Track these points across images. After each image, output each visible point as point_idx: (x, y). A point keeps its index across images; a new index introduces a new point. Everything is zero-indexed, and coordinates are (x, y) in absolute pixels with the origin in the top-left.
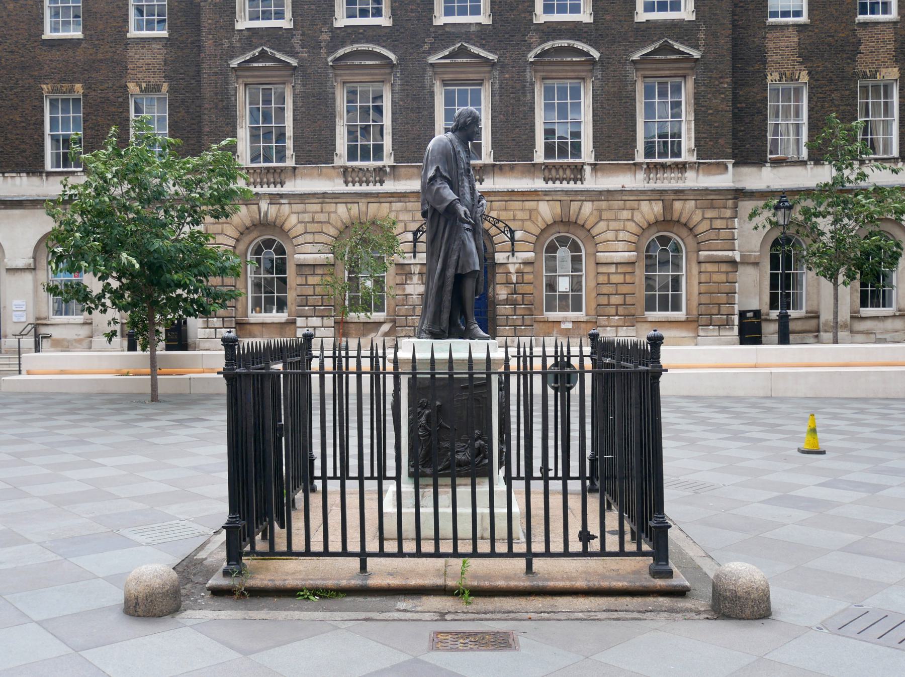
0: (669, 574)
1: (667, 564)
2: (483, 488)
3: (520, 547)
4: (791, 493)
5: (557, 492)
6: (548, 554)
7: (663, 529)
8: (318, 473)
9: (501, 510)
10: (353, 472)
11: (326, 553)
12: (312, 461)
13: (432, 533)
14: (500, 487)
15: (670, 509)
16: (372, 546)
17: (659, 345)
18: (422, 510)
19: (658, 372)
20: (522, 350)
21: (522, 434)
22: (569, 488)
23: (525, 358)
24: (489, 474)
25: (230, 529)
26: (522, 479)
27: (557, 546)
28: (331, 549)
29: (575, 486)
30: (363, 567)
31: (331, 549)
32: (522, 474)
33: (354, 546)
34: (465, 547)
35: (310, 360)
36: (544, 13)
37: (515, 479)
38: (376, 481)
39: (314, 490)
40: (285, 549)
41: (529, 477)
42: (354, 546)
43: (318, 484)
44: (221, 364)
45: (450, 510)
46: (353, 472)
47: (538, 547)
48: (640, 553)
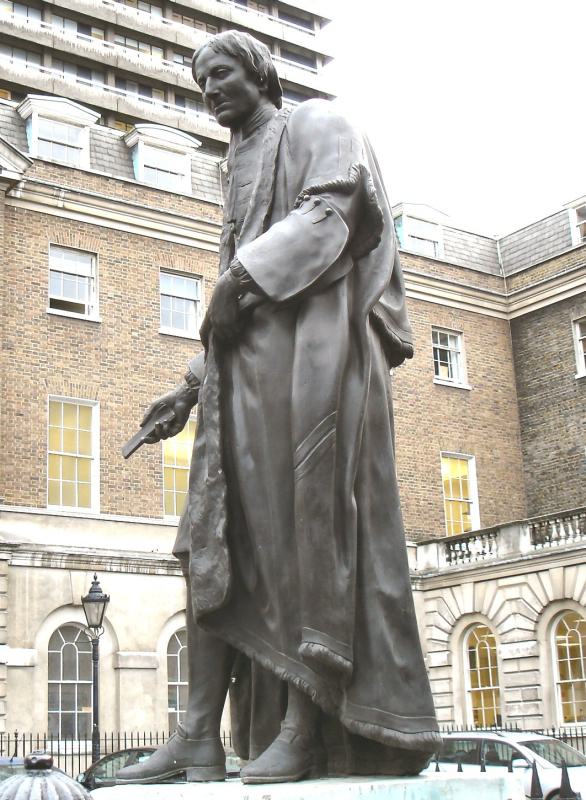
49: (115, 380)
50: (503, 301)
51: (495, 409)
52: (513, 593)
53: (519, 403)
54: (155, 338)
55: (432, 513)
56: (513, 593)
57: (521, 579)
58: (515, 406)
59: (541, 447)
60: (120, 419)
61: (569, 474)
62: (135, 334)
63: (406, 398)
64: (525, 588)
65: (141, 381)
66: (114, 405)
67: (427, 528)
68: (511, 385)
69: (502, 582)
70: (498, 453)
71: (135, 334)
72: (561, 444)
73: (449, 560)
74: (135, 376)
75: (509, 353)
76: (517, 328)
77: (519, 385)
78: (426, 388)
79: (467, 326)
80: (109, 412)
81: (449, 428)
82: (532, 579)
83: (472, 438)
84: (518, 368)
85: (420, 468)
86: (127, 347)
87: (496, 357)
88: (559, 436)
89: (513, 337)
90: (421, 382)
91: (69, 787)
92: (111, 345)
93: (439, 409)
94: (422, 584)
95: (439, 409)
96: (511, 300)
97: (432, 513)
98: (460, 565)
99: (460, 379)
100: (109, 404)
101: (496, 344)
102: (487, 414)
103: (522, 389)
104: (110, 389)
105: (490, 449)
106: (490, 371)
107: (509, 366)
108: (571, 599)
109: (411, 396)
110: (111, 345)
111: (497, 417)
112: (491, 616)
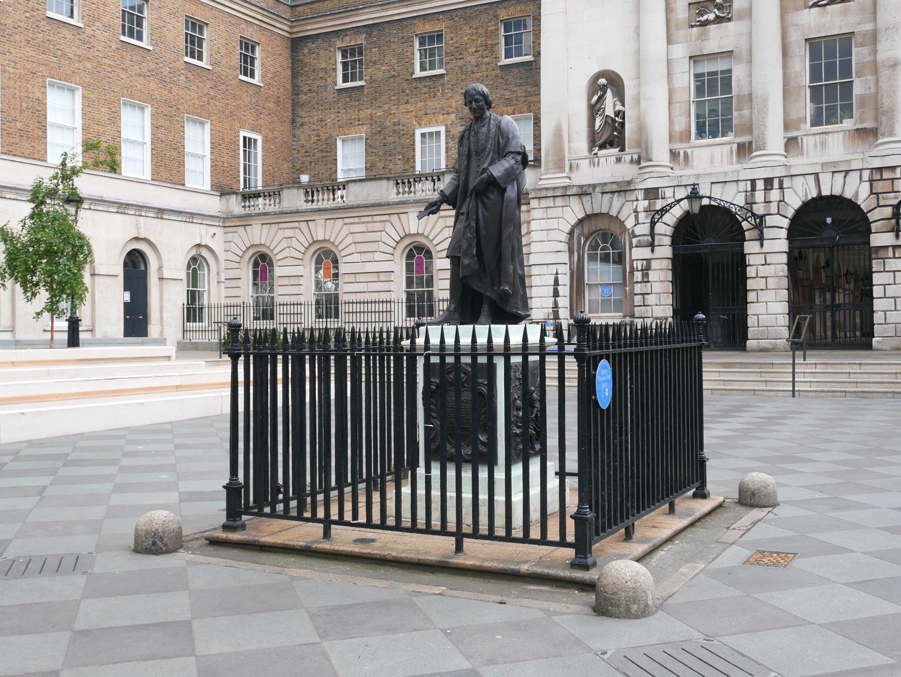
3: (321, 514)
16: (467, 528)
33: (452, 526)
42: (452, 526)
47: (467, 528)
49: (12, 50)
50: (289, 23)
51: (277, 102)
52: (288, 233)
53: (293, 100)
54: (43, 19)
55: (231, 172)
56: (288, 233)
57: (386, 218)
58: (290, 102)
59: (303, 134)
60: (15, 81)
61: (324, 154)
62: (28, 15)
63: (219, 88)
64: (388, 224)
65: (32, 53)
66: (12, 70)
67: (228, 183)
68: (289, 87)
69: (281, 226)
70: (277, 134)
71: (28, 15)
72: (321, 133)
73: (244, 207)
74: (27, 49)
75: (288, 63)
76: (296, 44)
77: (295, 86)
78: (233, 82)
79: (263, 39)
80: (7, 75)
81: (247, 113)
82: (394, 218)
83: (261, 122)
84: (295, 75)
85: (226, 140)
86: (22, 24)
87: (283, 60)
88: (320, 127)
89: (292, 51)
90: (231, 77)
91: (810, 487)
92: (9, 21)
93: (241, 98)
94: (224, 222)
95: (241, 98)
96: (294, 24)
97: (231, 172)
98: (252, 211)
99: (256, 81)
100: (7, 68)
101: (281, 54)
102: (272, 105)
103: (296, 90)
104: (8, 56)
105: (272, 130)
106: (276, 74)
107: (289, 72)
108: (333, 243)
109: (223, 87)
110: (9, 21)
111: (278, 108)
112: (336, 243)
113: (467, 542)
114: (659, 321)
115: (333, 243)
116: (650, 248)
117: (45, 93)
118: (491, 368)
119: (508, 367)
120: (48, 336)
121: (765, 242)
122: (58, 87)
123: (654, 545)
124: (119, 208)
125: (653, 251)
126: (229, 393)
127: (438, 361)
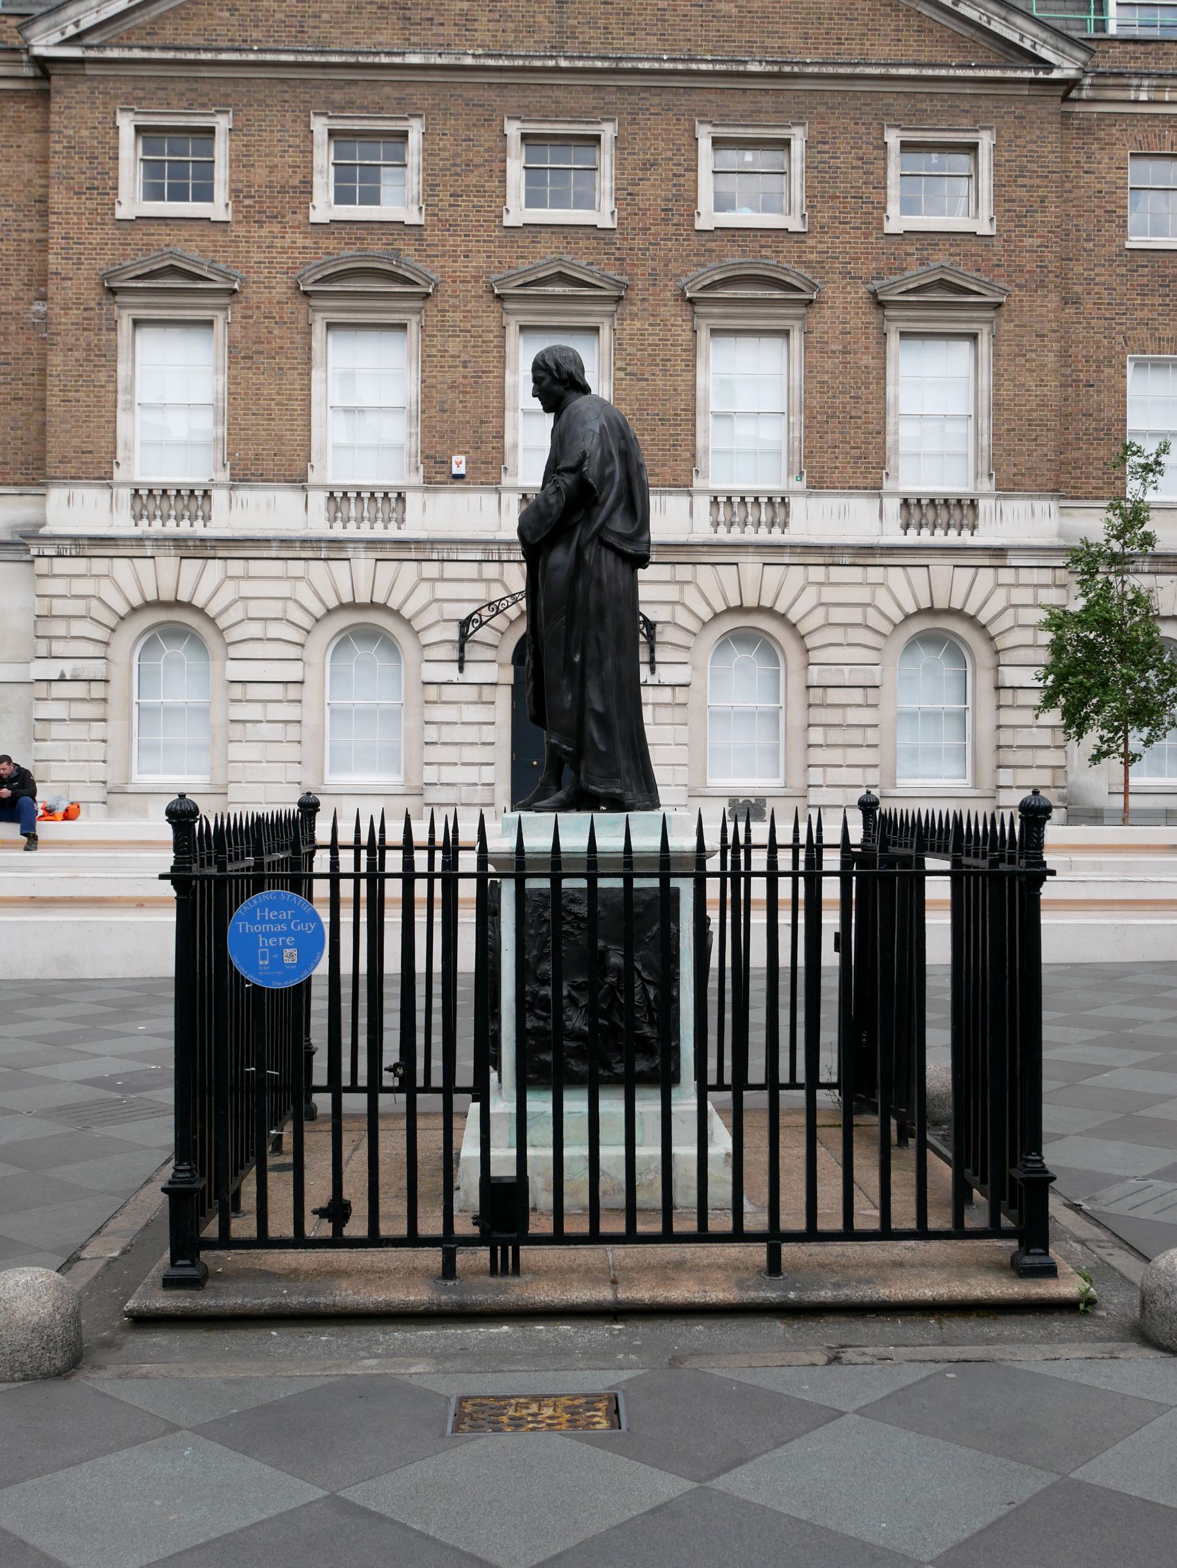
0: (1050, 1271)
1: (1047, 1253)
2: (648, 1106)
3: (430, 1224)
4: (1142, 1113)
5: (395, 1116)
6: (812, 1234)
7: (1041, 1183)
8: (320, 1077)
9: (685, 1150)
10: (756, 1071)
11: (849, 1234)
12: (310, 1053)
13: (621, 1199)
14: (685, 1102)
15: (1052, 1155)
16: (793, 1219)
17: (1041, 824)
18: (530, 1152)
19: (1041, 874)
20: (803, 827)
21: (728, 998)
22: (783, 1105)
23: (202, 866)
24: (667, 1080)
25: (176, 1194)
26: (436, 1090)
27: (830, 1218)
28: (859, 1224)
29: (827, 1099)
30: (774, 1266)
31: (859, 1224)
32: (801, 1078)
33: (756, 1219)
34: (577, 1224)
35: (312, 854)
36: (336, 203)
37: (348, 1090)
38: (365, 1096)
39: (312, 1115)
40: (289, 1232)
41: (740, 1084)
42: (756, 1219)
43: (322, 1102)
44: (166, 859)
45: (567, 1152)
46: (756, 1071)
47: (793, 1219)
48: (994, 1231)
108: (221, 632)
113: (788, 1251)
114: (450, 812)
115: (221, 632)
116: (456, 665)
117: (882, 356)
118: (669, 898)
119: (521, 895)
120: (1118, 802)
121: (467, 666)
122: (1153, 366)
123: (462, 1305)
124: (484, 551)
125: (461, 669)
126: (949, 921)
127: (549, 886)
